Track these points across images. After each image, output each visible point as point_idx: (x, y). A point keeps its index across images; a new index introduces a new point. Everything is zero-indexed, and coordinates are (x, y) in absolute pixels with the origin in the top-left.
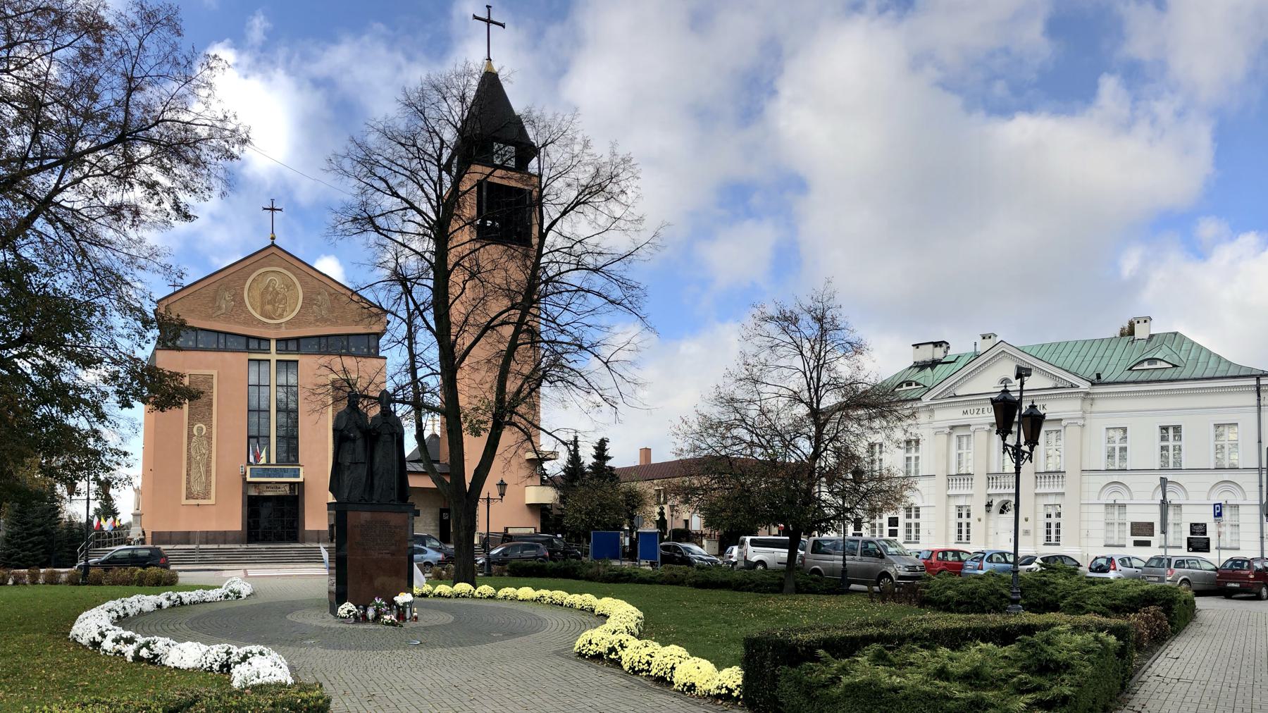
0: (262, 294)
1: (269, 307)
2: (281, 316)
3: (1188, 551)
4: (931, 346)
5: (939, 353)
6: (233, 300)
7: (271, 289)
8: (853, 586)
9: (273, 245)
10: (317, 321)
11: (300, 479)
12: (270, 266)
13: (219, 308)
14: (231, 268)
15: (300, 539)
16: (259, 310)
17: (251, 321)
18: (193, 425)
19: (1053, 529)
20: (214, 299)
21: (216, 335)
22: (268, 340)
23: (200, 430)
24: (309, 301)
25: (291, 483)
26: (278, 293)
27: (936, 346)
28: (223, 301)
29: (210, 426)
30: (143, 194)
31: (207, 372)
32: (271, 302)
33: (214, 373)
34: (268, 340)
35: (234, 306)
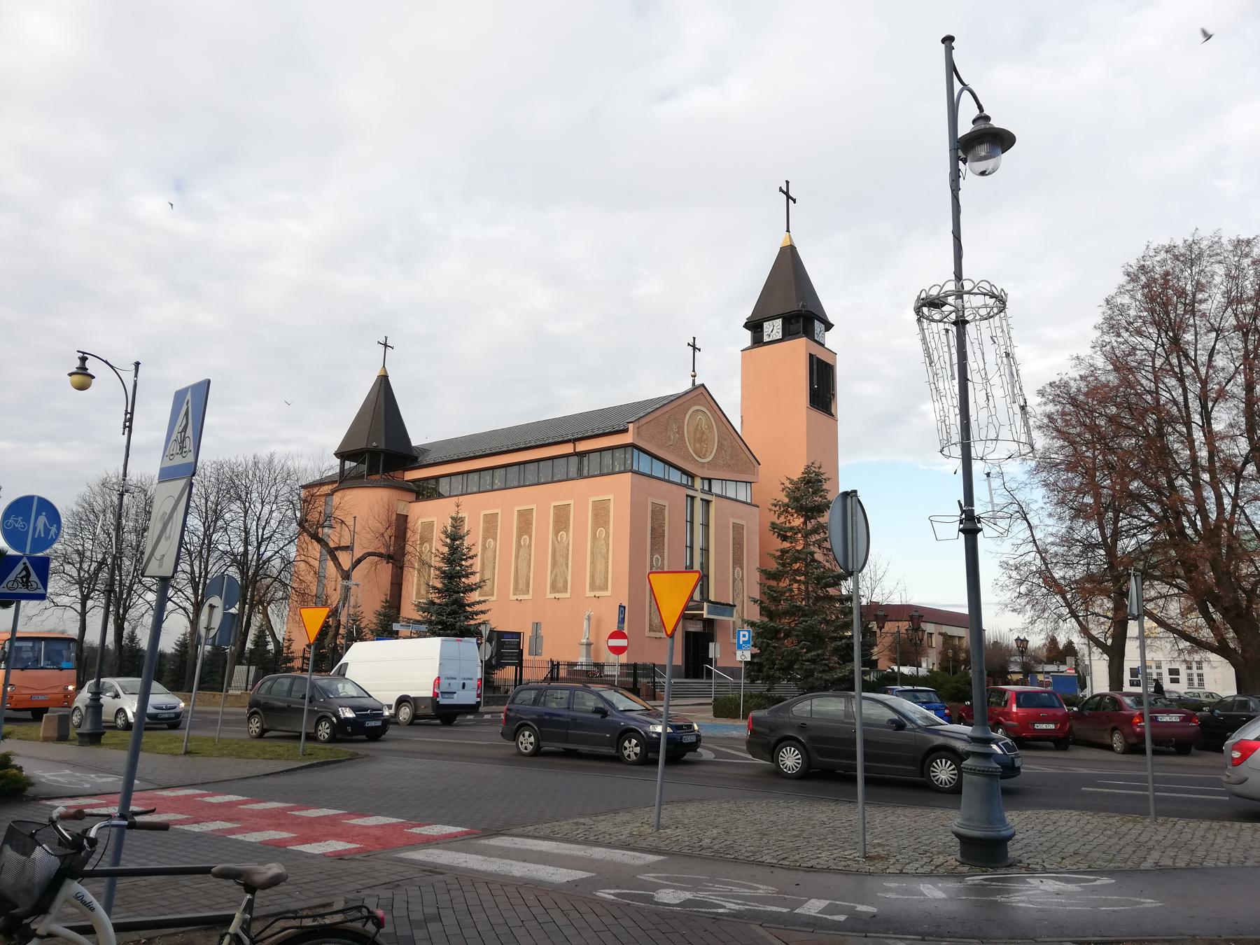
2: (705, 456)
17: (687, 457)
24: (720, 445)
31: (662, 503)
32: (700, 440)
34: (692, 476)
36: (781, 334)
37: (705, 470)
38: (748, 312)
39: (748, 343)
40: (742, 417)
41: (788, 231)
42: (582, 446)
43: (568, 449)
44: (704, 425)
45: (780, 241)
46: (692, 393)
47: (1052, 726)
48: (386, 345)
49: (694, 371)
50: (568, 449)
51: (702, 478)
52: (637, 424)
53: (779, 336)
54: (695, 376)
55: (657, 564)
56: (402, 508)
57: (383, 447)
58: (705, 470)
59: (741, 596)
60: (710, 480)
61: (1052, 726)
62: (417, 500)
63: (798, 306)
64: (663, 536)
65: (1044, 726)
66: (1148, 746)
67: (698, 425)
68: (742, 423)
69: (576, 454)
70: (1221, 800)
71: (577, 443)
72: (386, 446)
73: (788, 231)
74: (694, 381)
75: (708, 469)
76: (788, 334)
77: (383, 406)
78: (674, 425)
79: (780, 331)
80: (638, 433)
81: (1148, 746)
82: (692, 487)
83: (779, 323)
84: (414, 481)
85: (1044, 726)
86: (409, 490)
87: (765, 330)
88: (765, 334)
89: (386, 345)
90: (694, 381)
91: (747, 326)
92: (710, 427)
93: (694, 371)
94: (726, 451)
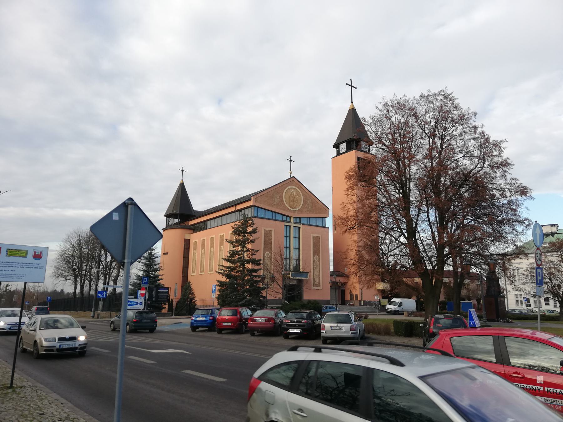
0: (289, 198)
1: (291, 203)
2: (296, 208)
3: (119, 331)
4: (550, 226)
5: (554, 229)
6: (279, 199)
7: (292, 196)
8: (299, 331)
9: (291, 177)
10: (307, 211)
11: (308, 279)
12: (293, 186)
13: (274, 201)
14: (279, 184)
15: (542, 321)
16: (288, 204)
17: (285, 209)
18: (265, 252)
19: (519, 302)
20: (273, 197)
21: (271, 213)
22: (290, 217)
23: (268, 254)
24: (305, 203)
25: (298, 280)
26: (295, 198)
27: (552, 226)
28: (276, 199)
29: (271, 253)
30: (412, 98)
31: (270, 229)
32: (293, 201)
33: (273, 230)
34: (290, 217)
35: (280, 201)
36: (346, 149)
37: (296, 214)
38: (334, 141)
39: (335, 154)
40: (332, 188)
41: (352, 102)
42: (239, 207)
43: (233, 209)
44: (295, 194)
45: (348, 107)
46: (289, 180)
47: (230, 324)
48: (291, 161)
49: (291, 171)
50: (233, 209)
51: (294, 217)
52: (255, 197)
53: (345, 150)
54: (291, 173)
55: (267, 256)
56: (187, 237)
57: (178, 212)
58: (296, 214)
59: (318, 268)
60: (300, 218)
61: (230, 324)
62: (194, 232)
63: (352, 136)
64: (271, 244)
65: (227, 324)
66: (539, 329)
67: (291, 194)
68: (332, 190)
69: (236, 211)
70: (141, 350)
71: (237, 206)
72: (180, 211)
73: (352, 102)
74: (291, 175)
75: (298, 213)
76: (349, 149)
77: (180, 196)
78: (277, 196)
79: (346, 148)
80: (256, 200)
81: (539, 329)
82: (290, 222)
83: (345, 144)
84: (194, 225)
85: (227, 324)
86: (190, 229)
87: (340, 148)
88: (340, 150)
89: (291, 161)
90: (291, 175)
91: (334, 146)
92: (298, 195)
93: (291, 171)
94: (308, 205)
